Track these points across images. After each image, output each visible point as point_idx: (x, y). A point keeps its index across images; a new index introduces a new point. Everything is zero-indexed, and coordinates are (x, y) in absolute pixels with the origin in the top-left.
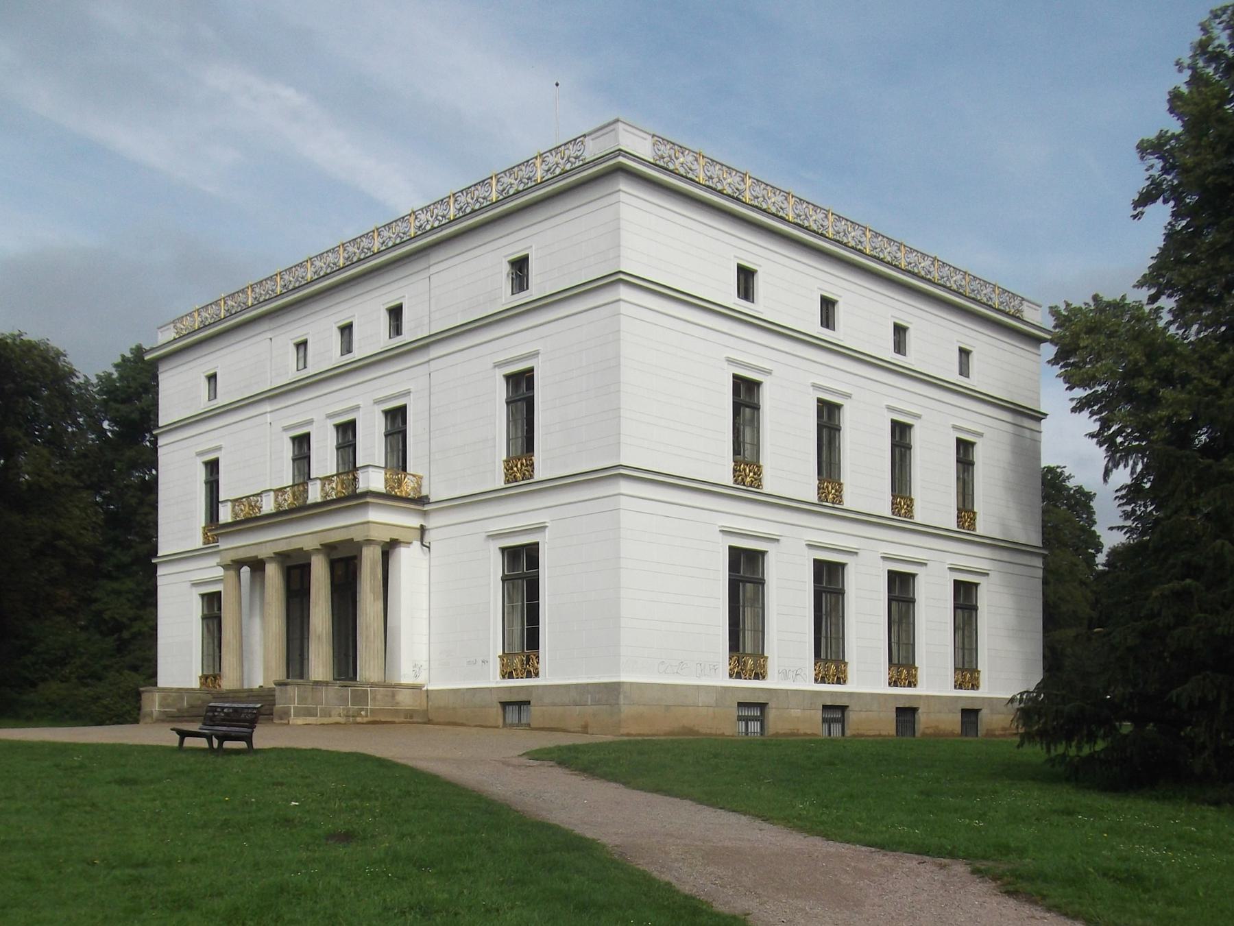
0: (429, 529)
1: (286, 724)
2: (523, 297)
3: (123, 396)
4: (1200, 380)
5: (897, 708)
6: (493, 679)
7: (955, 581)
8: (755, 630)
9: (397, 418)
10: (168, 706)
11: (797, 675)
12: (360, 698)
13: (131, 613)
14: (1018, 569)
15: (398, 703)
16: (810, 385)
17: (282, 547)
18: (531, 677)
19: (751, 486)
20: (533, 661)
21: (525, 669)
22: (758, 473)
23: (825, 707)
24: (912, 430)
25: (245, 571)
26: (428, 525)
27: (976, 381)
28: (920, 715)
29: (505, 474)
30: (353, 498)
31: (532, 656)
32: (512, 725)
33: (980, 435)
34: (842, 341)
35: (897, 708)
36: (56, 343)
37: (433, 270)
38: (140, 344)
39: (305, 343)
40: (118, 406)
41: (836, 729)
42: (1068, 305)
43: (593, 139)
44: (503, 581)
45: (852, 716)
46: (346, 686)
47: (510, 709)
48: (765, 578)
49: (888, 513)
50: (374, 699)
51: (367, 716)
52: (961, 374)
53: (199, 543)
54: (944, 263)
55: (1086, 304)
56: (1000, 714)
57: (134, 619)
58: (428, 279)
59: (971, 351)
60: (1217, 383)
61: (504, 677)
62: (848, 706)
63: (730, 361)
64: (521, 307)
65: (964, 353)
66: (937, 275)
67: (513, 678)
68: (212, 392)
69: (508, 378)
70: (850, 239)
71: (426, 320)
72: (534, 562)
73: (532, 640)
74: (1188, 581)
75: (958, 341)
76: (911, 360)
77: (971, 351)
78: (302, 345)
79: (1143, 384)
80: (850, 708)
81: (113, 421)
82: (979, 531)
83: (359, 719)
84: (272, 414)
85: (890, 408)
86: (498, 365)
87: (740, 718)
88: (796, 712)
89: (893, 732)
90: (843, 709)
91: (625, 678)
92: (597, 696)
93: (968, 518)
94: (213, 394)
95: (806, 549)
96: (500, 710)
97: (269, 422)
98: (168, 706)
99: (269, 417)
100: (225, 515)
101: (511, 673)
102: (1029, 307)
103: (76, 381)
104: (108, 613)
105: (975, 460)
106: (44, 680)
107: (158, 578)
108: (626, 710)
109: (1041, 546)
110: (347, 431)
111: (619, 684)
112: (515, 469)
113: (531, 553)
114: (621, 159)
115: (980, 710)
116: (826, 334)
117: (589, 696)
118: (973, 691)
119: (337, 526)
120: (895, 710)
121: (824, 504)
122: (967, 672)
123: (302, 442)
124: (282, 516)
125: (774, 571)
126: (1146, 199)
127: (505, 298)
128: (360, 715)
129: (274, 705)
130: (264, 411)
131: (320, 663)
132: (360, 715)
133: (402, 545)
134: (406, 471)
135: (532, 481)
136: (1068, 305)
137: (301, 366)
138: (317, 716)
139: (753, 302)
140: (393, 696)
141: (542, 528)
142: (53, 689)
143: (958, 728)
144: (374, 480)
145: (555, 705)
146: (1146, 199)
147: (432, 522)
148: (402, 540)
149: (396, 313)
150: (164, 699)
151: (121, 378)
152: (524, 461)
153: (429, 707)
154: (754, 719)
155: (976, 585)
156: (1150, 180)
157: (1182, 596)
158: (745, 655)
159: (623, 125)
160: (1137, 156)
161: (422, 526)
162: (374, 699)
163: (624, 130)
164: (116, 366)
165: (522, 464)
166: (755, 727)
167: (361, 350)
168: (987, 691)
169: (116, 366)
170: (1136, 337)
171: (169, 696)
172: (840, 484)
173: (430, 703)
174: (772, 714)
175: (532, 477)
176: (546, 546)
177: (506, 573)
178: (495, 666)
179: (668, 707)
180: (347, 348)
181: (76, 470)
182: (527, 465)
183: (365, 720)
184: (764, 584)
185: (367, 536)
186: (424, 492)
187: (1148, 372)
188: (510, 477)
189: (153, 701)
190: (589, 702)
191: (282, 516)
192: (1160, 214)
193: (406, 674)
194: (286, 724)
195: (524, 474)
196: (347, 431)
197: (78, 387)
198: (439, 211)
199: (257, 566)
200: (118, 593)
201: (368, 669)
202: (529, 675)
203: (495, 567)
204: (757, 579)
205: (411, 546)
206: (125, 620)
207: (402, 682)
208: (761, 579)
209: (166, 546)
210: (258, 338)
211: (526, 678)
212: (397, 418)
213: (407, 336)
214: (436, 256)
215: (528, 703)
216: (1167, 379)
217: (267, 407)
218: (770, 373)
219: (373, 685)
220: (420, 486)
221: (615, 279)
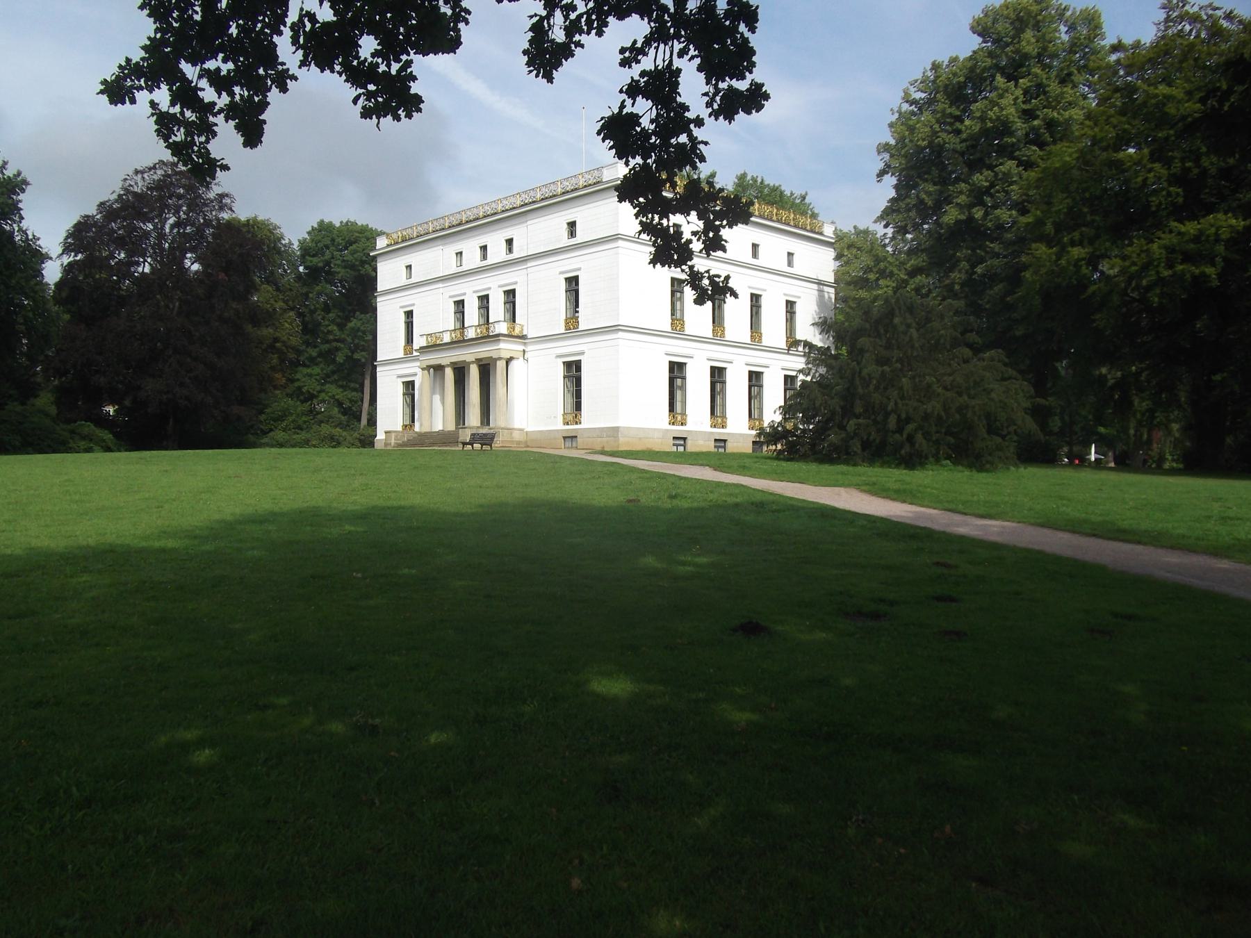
3: (314, 252)
4: (898, 275)
6: (559, 425)
8: (682, 402)
9: (510, 295)
10: (398, 440)
13: (318, 388)
17: (454, 360)
20: (579, 416)
22: (683, 325)
23: (716, 440)
25: (432, 370)
26: (526, 350)
27: (798, 269)
30: (488, 337)
32: (568, 448)
36: (275, 220)
37: (529, 223)
38: (331, 222)
39: (461, 253)
40: (311, 259)
41: (721, 450)
45: (729, 445)
47: (567, 439)
49: (670, 330)
50: (503, 435)
53: (402, 355)
57: (319, 392)
65: (790, 255)
68: (408, 274)
71: (525, 247)
72: (579, 368)
73: (578, 406)
76: (762, 261)
78: (460, 254)
81: (306, 268)
86: (561, 273)
87: (674, 445)
88: (701, 442)
89: (751, 451)
90: (725, 441)
94: (410, 276)
96: (563, 441)
98: (398, 440)
100: (419, 342)
101: (568, 422)
103: (283, 242)
104: (306, 388)
106: (271, 430)
107: (378, 373)
108: (622, 440)
110: (484, 300)
111: (618, 427)
113: (487, 297)
116: (754, 262)
119: (484, 351)
123: (460, 305)
124: (454, 344)
125: (690, 372)
126: (881, 174)
127: (565, 241)
137: (459, 265)
140: (511, 434)
142: (279, 435)
144: (502, 328)
145: (589, 437)
147: (529, 348)
149: (510, 242)
150: (396, 436)
151: (312, 240)
154: (681, 445)
155: (762, 373)
158: (677, 413)
160: (877, 153)
161: (524, 351)
162: (503, 435)
164: (309, 233)
166: (681, 449)
167: (492, 259)
169: (309, 233)
174: (689, 442)
175: (578, 328)
178: (560, 419)
179: (640, 438)
180: (484, 257)
181: (286, 299)
183: (499, 445)
186: (524, 333)
187: (875, 270)
189: (391, 438)
191: (454, 344)
192: (890, 180)
193: (517, 423)
196: (484, 300)
197: (285, 246)
198: (532, 194)
199: (439, 369)
200: (310, 375)
202: (576, 423)
203: (560, 370)
206: (315, 393)
209: (381, 355)
210: (436, 248)
212: (510, 295)
213: (516, 254)
214: (530, 216)
215: (576, 437)
216: (883, 274)
217: (440, 285)
219: (502, 429)
220: (522, 329)
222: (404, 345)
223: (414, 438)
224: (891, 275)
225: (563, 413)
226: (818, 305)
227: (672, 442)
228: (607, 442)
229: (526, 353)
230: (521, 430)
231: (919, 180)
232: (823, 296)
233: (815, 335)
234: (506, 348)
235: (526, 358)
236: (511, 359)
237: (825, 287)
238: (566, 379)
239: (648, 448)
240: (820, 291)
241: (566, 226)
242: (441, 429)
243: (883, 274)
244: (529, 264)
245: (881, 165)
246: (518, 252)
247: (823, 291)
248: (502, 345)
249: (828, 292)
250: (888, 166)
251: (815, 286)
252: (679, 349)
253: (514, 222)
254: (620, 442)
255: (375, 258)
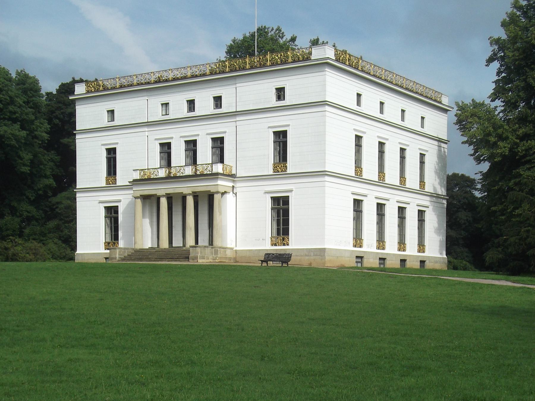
0: (236, 187)
1: (196, 262)
2: (192, 114)
5: (401, 260)
6: (102, 250)
7: (418, 210)
10: (121, 255)
11: (372, 246)
12: (216, 252)
14: (438, 205)
15: (226, 255)
16: (376, 136)
18: (285, 246)
19: (359, 176)
21: (282, 243)
24: (406, 151)
27: (427, 130)
28: (407, 262)
29: (273, 169)
31: (286, 238)
33: (427, 151)
34: (385, 118)
35: (401, 260)
37: (238, 85)
42: (463, 102)
43: (314, 50)
44: (272, 209)
46: (212, 248)
48: (363, 210)
51: (218, 260)
52: (380, 113)
53: (104, 184)
54: (417, 83)
55: (470, 103)
56: (432, 263)
58: (235, 88)
59: (425, 118)
60: (518, 141)
61: (272, 245)
62: (363, 257)
63: (355, 130)
64: (282, 107)
66: (415, 88)
67: (277, 246)
69: (275, 133)
70: (389, 78)
74: (530, 228)
75: (380, 99)
77: (425, 118)
79: (492, 139)
80: (387, 259)
82: (426, 190)
83: (216, 261)
84: (148, 132)
85: (400, 143)
91: (326, 246)
92: (315, 253)
93: (359, 170)
95: (375, 199)
97: (147, 135)
98: (121, 255)
99: (147, 133)
102: (444, 97)
105: (425, 161)
108: (327, 258)
109: (446, 195)
111: (325, 249)
112: (110, 180)
114: (328, 61)
115: (425, 261)
117: (312, 253)
118: (360, 248)
120: (400, 260)
121: (380, 181)
122: (381, 241)
126: (490, 60)
127: (104, 121)
128: (216, 259)
129: (190, 255)
130: (145, 130)
131: (203, 240)
132: (216, 259)
133: (227, 193)
134: (224, 163)
135: (286, 173)
136: (463, 102)
138: (205, 259)
139: (360, 106)
140: (225, 252)
141: (291, 191)
143: (419, 267)
146: (490, 60)
147: (238, 185)
148: (228, 192)
150: (120, 252)
152: (282, 165)
153: (237, 256)
155: (425, 211)
156: (493, 52)
157: (528, 231)
159: (327, 46)
161: (233, 186)
163: (328, 48)
165: (112, 179)
166: (359, 265)
168: (428, 253)
170: (489, 120)
171: (121, 251)
172: (384, 174)
173: (237, 255)
175: (286, 171)
176: (293, 197)
177: (273, 206)
178: (269, 241)
182: (284, 167)
184: (362, 212)
185: (218, 190)
186: (234, 172)
188: (275, 170)
190: (312, 255)
194: (196, 262)
195: (113, 183)
201: (217, 242)
202: (284, 245)
204: (360, 210)
205: (230, 194)
207: (228, 247)
208: (361, 210)
209: (81, 182)
211: (283, 246)
214: (238, 80)
216: (501, 138)
217: (146, 129)
218: (365, 133)
219: (220, 248)
221: (324, 103)
222: (105, 176)
223: (132, 253)
224: (507, 138)
225: (270, 236)
226: (438, 157)
227: (355, 260)
228: (314, 260)
229: (235, 189)
230: (232, 249)
231: (527, 69)
232: (441, 151)
233: (436, 180)
234: (223, 184)
235: (235, 192)
236: (225, 192)
237: (442, 144)
238: (378, 215)
239: (342, 264)
240: (439, 146)
241: (275, 91)
242: (150, 246)
243: (501, 138)
244: (238, 118)
245: (490, 53)
246: (225, 108)
247: (441, 147)
248: (220, 182)
249: (444, 148)
250: (495, 54)
251: (436, 143)
252: (360, 188)
253: (214, 84)
254: (326, 260)
255: (73, 102)
